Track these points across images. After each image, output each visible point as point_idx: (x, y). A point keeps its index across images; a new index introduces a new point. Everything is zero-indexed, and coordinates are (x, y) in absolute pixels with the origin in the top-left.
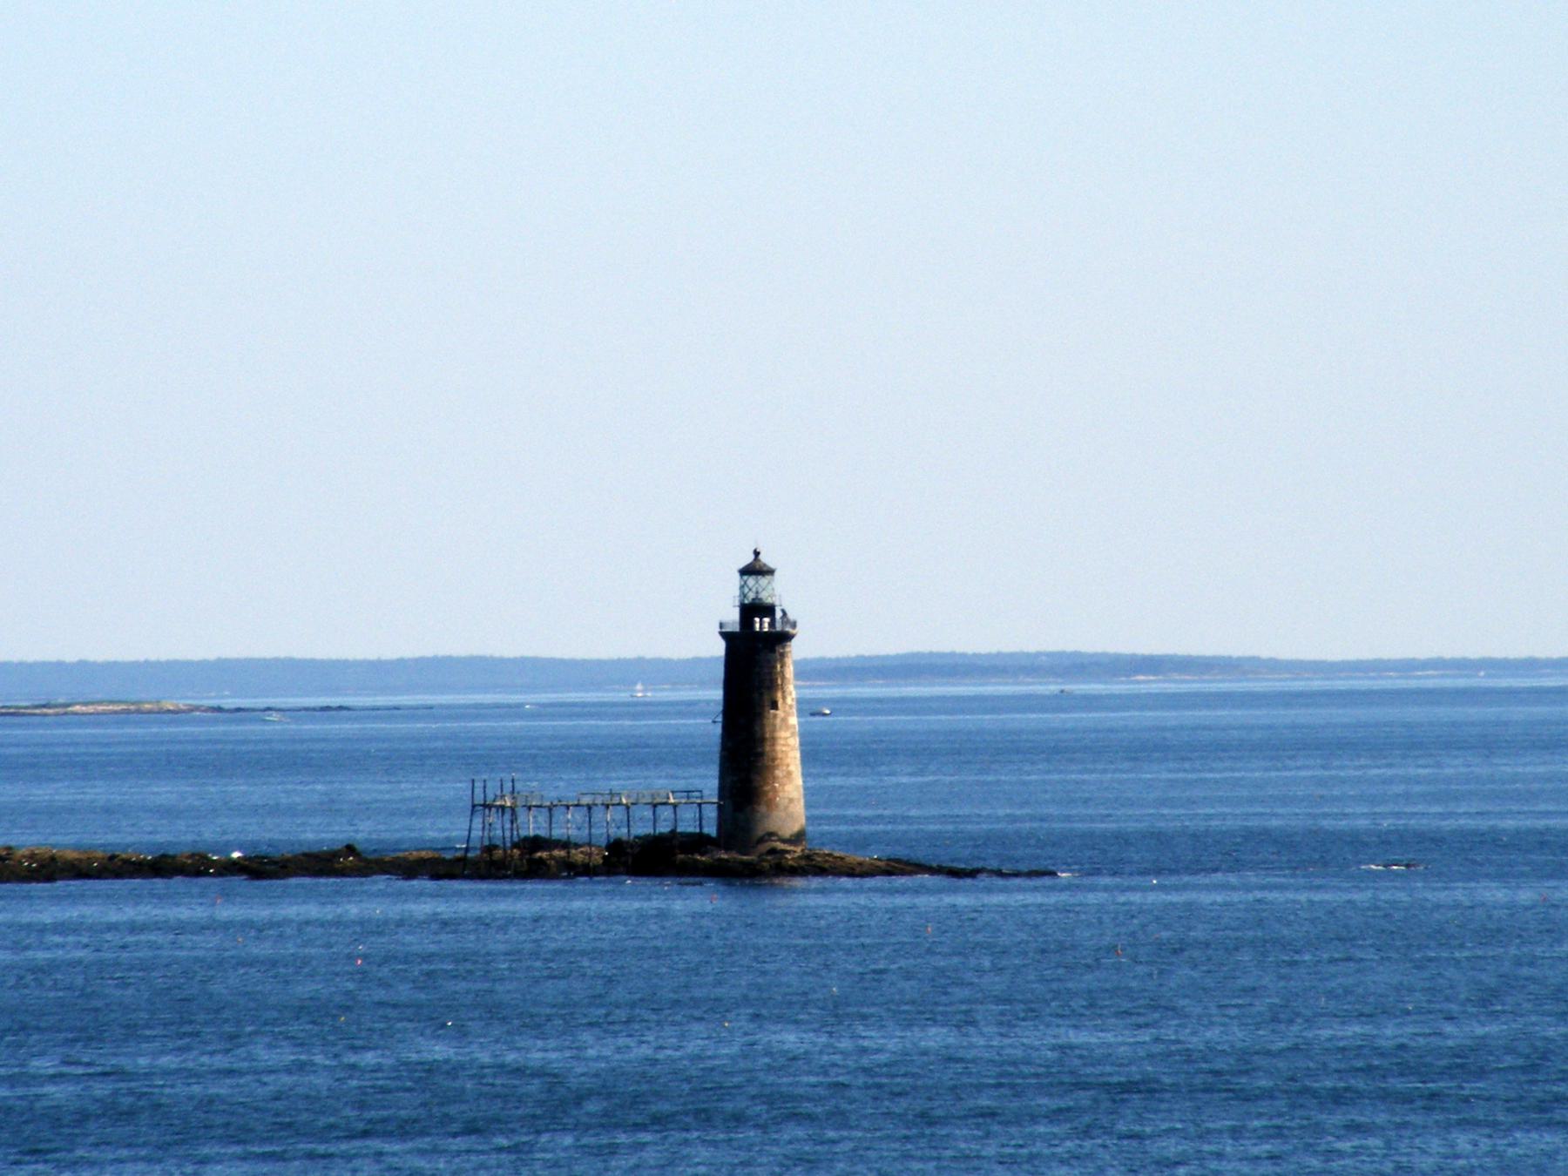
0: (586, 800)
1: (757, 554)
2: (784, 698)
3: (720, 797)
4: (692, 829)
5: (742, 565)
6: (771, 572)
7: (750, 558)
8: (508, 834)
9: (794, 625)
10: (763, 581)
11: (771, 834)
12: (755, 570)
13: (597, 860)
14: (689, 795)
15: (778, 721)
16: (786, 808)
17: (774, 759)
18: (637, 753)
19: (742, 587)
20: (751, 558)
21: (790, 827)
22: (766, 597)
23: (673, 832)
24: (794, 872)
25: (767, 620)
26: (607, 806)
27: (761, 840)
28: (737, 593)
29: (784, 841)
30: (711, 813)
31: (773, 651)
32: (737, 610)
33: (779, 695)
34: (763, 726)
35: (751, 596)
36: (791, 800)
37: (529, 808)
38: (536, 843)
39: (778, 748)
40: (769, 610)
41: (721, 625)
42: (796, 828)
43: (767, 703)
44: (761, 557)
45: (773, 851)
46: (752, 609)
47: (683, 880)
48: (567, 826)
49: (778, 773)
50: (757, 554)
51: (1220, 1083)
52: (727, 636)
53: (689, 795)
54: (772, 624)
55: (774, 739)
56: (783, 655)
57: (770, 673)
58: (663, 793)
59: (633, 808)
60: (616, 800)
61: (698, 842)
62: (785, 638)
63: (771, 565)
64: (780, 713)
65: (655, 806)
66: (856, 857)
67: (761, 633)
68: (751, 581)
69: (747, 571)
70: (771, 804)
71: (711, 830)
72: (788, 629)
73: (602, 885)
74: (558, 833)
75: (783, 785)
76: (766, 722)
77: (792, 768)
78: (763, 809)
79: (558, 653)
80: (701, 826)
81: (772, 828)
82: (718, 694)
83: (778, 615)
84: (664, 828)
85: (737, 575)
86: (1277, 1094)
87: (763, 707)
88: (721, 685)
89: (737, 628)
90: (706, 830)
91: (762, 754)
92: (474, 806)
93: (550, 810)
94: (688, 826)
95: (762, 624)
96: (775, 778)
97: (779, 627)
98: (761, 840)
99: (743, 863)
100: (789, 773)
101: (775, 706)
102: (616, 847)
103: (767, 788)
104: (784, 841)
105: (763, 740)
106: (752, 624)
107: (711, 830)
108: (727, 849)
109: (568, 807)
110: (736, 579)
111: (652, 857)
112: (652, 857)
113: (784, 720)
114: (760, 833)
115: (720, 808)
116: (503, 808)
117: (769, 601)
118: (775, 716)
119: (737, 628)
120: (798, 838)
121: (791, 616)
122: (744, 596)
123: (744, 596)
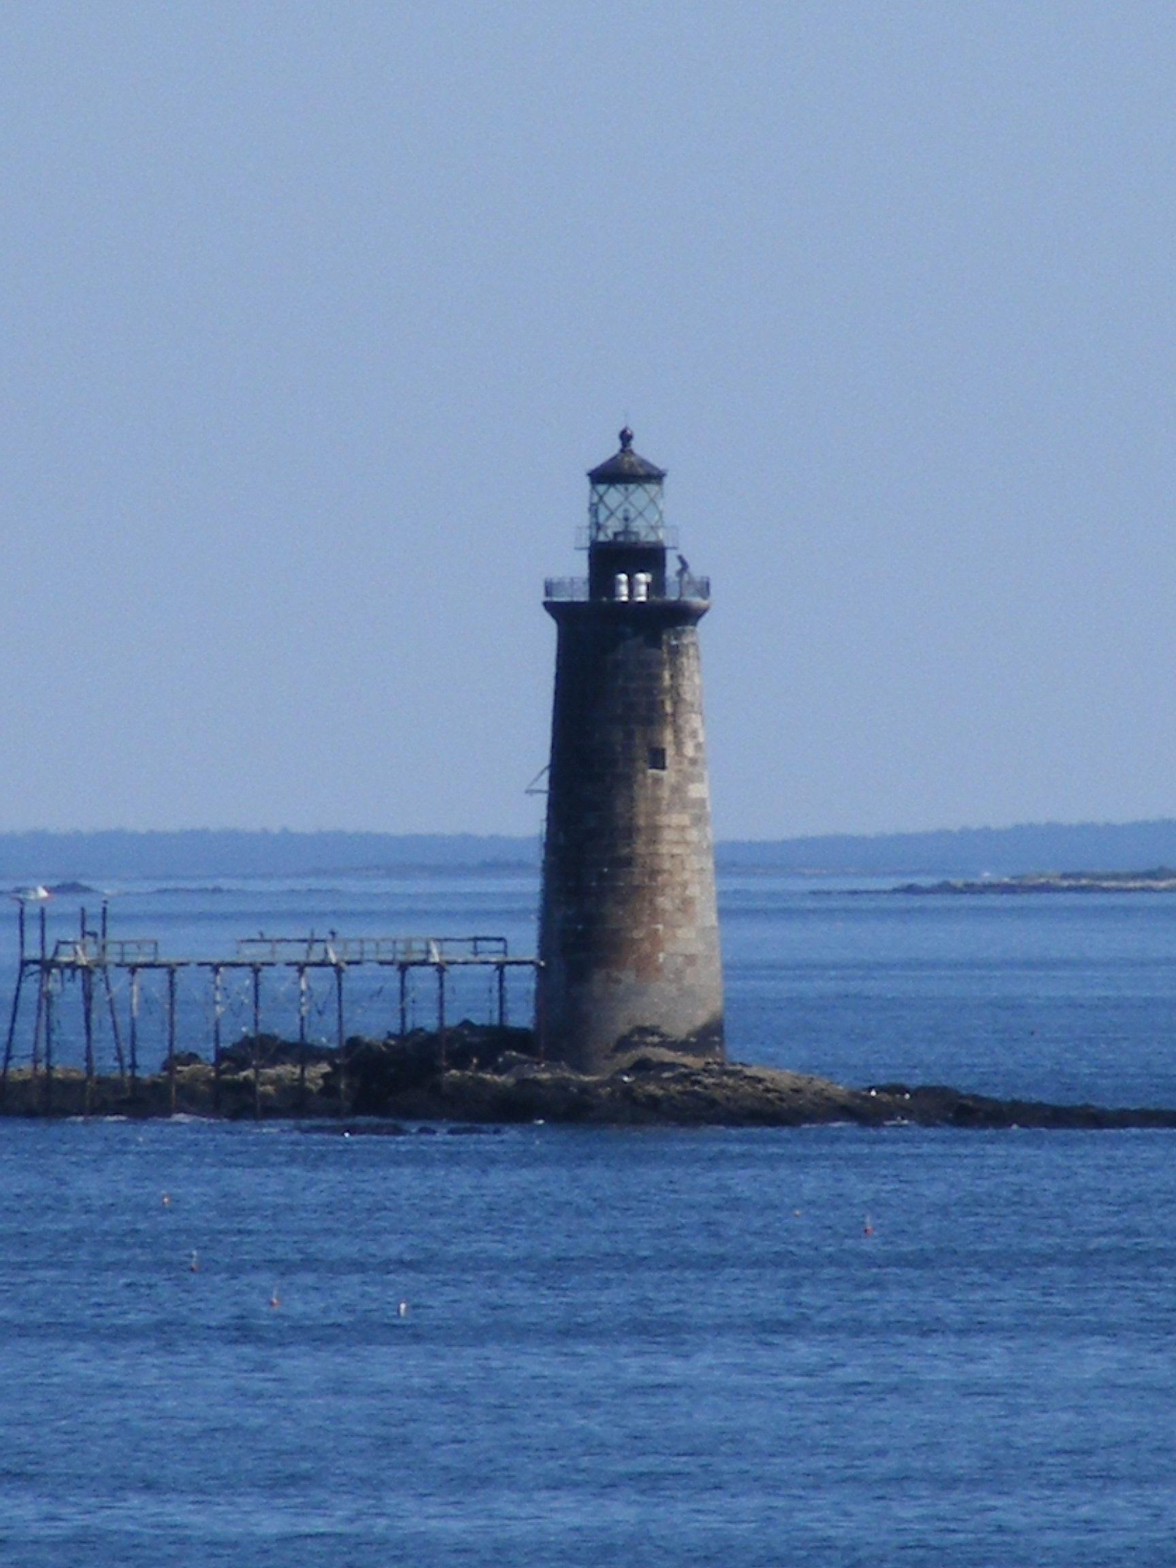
1: (625, 437)
2: (679, 744)
3: (543, 955)
5: (598, 459)
6: (654, 476)
9: (704, 589)
10: (639, 495)
11: (644, 1031)
15: (665, 793)
16: (679, 974)
17: (654, 873)
18: (492, 868)
19: (594, 510)
20: (617, 445)
21: (687, 1019)
22: (644, 533)
25: (643, 577)
28: (585, 518)
30: (523, 982)
31: (656, 642)
32: (584, 555)
33: (668, 736)
35: (613, 527)
36: (691, 959)
37: (133, 968)
39: (664, 849)
40: (650, 557)
41: (549, 588)
42: (701, 1017)
43: (641, 752)
44: (635, 445)
46: (612, 556)
49: (664, 902)
50: (625, 437)
53: (480, 952)
54: (657, 586)
55: (655, 830)
58: (419, 946)
61: (496, 1041)
62: (684, 615)
63: (658, 462)
64: (669, 775)
65: (403, 967)
66: (778, 1069)
67: (632, 607)
68: (614, 495)
70: (646, 966)
71: (522, 1017)
72: (697, 601)
76: (638, 791)
77: (694, 891)
78: (628, 977)
79: (551, 669)
85: (586, 482)
86: (199, 1363)
87: (631, 761)
89: (582, 596)
92: (24, 963)
93: (256, 971)
94: (470, 1002)
95: (634, 588)
96: (656, 914)
97: (672, 596)
100: (686, 904)
101: (657, 759)
105: (630, 832)
106: (612, 589)
108: (553, 1056)
112: (397, 1083)
116: (72, 966)
118: (657, 781)
119: (582, 596)
120: (709, 1036)
121: (697, 571)
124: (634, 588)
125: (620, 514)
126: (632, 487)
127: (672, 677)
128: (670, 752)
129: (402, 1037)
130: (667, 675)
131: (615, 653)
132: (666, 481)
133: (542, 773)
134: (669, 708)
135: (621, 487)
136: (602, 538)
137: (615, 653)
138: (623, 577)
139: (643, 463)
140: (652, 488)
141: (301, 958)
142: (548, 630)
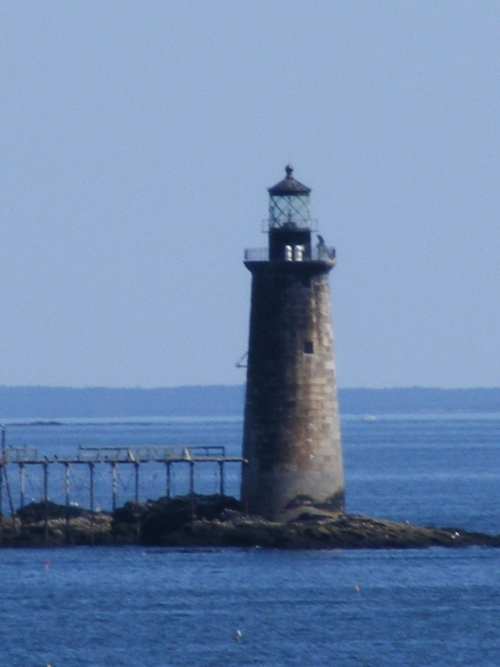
0: (87, 455)
1: (289, 170)
2: (320, 340)
3: (246, 453)
5: (273, 183)
6: (305, 192)
7: (280, 176)
9: (333, 254)
10: (296, 201)
11: (304, 498)
12: (286, 189)
13: (106, 528)
15: (313, 366)
16: (321, 468)
17: (307, 410)
19: (272, 209)
21: (325, 491)
24: (326, 541)
26: (113, 464)
27: (292, 505)
28: (266, 215)
29: (319, 506)
31: (307, 284)
34: (294, 372)
35: (283, 219)
36: (327, 458)
37: (21, 464)
38: (44, 509)
39: (313, 397)
40: (303, 237)
41: (246, 253)
44: (295, 175)
45: (305, 517)
46: (284, 236)
47: (153, 549)
48: (64, 487)
50: (289, 170)
52: (252, 266)
54: (307, 253)
55: (307, 387)
56: (318, 289)
60: (123, 456)
61: (219, 504)
62: (321, 269)
64: (315, 357)
65: (168, 463)
67: (295, 265)
68: (282, 202)
69: (277, 191)
70: (304, 463)
71: (234, 491)
73: (114, 555)
74: (56, 497)
75: (318, 440)
76: (298, 366)
77: (329, 420)
78: (293, 468)
80: (222, 490)
81: (306, 492)
82: (241, 418)
83: (314, 241)
84: (180, 490)
85: (267, 195)
89: (264, 256)
90: (228, 493)
91: (293, 404)
94: (206, 482)
95: (295, 253)
96: (309, 433)
97: (315, 256)
98: (292, 505)
99: (269, 530)
100: (325, 427)
101: (309, 348)
102: (123, 515)
103: (299, 444)
104: (319, 506)
105: (294, 388)
106: (283, 252)
107: (234, 491)
108: (253, 512)
109: (66, 464)
110: (265, 200)
111: (163, 525)
112: (163, 525)
113: (320, 365)
114: (290, 495)
118: (309, 360)
119: (264, 256)
120: (337, 501)
121: (329, 244)
122: (274, 219)
124: (295, 253)
125: (286, 212)
126: (292, 197)
127: (317, 303)
128: (315, 344)
131: (285, 290)
132: (312, 194)
134: (314, 320)
135: (286, 198)
136: (277, 226)
137: (285, 290)
139: (299, 184)
142: (247, 276)
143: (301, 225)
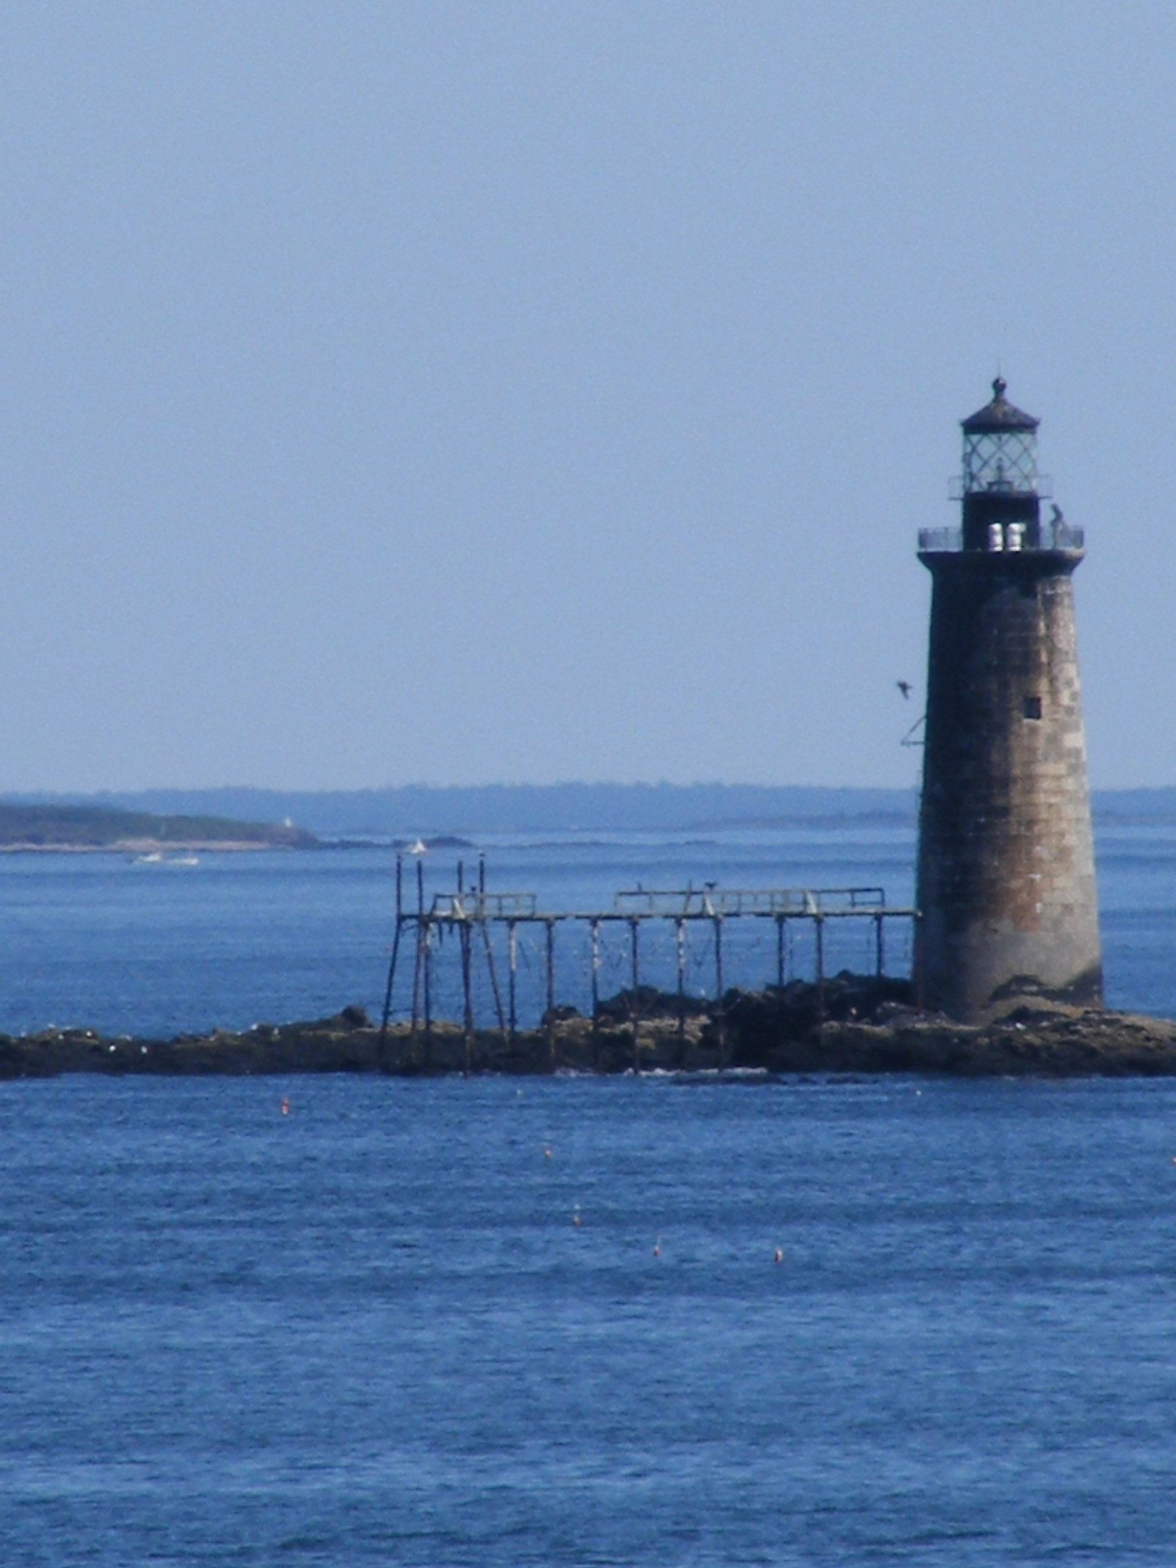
1: (999, 387)
2: (1054, 693)
4: (863, 967)
6: (1026, 425)
7: (985, 397)
8: (403, 993)
10: (1013, 444)
11: (1022, 980)
12: (994, 422)
14: (868, 908)
15: (1041, 743)
16: (1057, 924)
17: (1031, 823)
19: (967, 459)
20: (990, 395)
21: (1064, 969)
23: (821, 979)
25: (1016, 527)
28: (958, 469)
33: (1043, 686)
34: (1007, 751)
35: (987, 476)
36: (1068, 908)
39: (1042, 798)
40: (1023, 507)
41: (923, 539)
42: (1079, 966)
43: (1016, 701)
44: (1008, 395)
46: (986, 506)
49: (1040, 851)
50: (999, 387)
51: (879, 936)
53: (868, 908)
54: (1031, 536)
55: (1031, 780)
57: (1025, 642)
59: (726, 923)
60: (694, 909)
61: (875, 992)
65: (781, 918)
68: (987, 445)
69: (979, 425)
70: (1023, 916)
71: (900, 968)
75: (1049, 876)
77: (1071, 840)
83: (1046, 516)
85: (960, 430)
88: (915, 823)
89: (954, 545)
92: (401, 918)
95: (1007, 537)
97: (1046, 544)
100: (1063, 854)
101: (1033, 708)
105: (1006, 782)
112: (781, 1032)
113: (1054, 739)
114: (1000, 977)
115: (920, 923)
117: (1025, 488)
118: (1034, 731)
119: (954, 545)
120: (1087, 985)
121: (1071, 520)
122: (972, 477)
123: (972, 477)
124: (1007, 537)
125: (993, 463)
126: (1005, 437)
127: (1048, 627)
129: (779, 989)
130: (1042, 625)
131: (990, 603)
133: (920, 721)
134: (1044, 658)
135: (994, 437)
136: (976, 488)
137: (990, 603)
138: (997, 527)
140: (1026, 438)
141: (679, 911)
142: (923, 580)
143: (1020, 486)
